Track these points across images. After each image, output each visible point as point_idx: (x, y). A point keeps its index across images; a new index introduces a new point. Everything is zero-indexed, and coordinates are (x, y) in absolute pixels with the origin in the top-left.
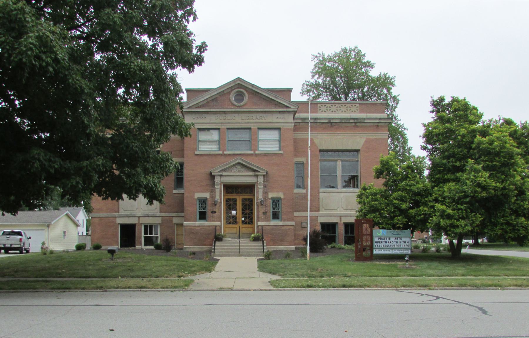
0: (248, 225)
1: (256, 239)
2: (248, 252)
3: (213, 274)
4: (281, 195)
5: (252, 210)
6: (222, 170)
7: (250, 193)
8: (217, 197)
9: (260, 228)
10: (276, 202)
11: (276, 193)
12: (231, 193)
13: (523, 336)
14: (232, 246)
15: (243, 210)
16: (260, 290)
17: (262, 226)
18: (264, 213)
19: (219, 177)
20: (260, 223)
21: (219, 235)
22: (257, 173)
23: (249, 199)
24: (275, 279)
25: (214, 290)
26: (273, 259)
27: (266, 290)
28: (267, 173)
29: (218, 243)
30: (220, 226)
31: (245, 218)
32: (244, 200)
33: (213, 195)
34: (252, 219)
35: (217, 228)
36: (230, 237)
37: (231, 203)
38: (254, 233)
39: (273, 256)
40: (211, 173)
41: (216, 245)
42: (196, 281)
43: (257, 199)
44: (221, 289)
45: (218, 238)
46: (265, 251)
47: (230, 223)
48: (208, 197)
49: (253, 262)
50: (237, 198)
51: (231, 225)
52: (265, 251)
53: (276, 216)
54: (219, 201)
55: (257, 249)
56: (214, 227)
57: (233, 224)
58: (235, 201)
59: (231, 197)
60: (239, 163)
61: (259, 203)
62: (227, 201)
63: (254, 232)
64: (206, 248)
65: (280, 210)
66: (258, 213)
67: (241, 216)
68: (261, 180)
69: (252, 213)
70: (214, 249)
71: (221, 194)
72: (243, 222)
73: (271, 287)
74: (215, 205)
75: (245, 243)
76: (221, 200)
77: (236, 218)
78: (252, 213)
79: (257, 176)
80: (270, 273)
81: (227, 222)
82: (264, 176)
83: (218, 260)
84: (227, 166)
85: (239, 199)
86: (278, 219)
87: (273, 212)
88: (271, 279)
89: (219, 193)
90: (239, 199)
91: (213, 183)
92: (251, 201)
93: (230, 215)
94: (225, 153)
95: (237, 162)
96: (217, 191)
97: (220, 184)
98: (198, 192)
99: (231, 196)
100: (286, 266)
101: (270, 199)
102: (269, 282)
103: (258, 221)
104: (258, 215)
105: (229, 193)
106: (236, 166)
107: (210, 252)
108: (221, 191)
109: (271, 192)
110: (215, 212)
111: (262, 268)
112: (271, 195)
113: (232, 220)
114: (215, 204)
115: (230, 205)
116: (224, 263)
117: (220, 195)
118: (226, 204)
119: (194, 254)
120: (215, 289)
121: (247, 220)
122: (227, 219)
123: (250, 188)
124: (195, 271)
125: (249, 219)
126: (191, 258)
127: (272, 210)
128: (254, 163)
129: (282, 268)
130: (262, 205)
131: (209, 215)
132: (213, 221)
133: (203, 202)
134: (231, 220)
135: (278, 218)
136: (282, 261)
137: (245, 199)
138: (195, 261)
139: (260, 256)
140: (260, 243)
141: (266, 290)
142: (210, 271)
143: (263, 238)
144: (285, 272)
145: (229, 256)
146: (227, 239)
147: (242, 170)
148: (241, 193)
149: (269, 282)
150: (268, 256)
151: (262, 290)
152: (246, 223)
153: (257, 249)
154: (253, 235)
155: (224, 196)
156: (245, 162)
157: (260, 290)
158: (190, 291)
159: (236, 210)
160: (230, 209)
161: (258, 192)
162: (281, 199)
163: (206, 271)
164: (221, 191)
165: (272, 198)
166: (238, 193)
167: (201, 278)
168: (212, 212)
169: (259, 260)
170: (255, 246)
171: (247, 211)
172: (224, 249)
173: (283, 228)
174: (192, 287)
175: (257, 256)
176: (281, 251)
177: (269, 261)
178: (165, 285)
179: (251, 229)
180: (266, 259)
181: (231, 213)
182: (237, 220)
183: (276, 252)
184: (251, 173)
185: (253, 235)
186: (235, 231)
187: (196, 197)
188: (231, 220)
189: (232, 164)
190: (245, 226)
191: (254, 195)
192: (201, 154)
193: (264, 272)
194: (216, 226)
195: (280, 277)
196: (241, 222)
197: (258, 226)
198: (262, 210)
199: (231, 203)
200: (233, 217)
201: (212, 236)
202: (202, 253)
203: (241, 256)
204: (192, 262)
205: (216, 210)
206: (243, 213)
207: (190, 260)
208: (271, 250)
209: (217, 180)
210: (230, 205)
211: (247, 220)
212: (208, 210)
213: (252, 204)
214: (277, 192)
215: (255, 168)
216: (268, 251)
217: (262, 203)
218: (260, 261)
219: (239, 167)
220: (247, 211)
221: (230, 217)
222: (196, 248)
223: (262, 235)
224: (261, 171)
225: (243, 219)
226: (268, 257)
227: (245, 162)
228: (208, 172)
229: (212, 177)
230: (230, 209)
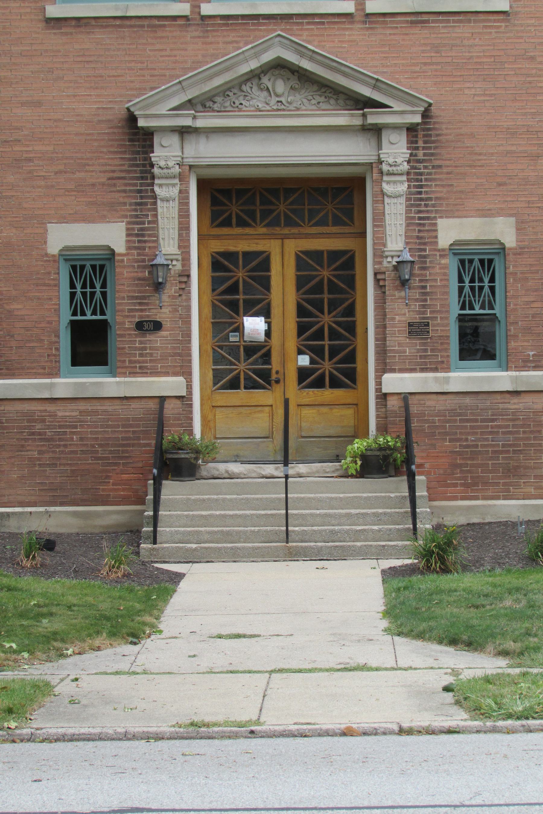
0: (328, 394)
1: (374, 465)
2: (332, 536)
3: (151, 652)
4: (503, 231)
5: (350, 311)
6: (190, 103)
7: (337, 222)
8: (168, 246)
9: (393, 403)
10: (479, 267)
11: (477, 221)
12: (242, 223)
13: (190, 810)
14: (247, 504)
15: (301, 311)
16: (402, 731)
17: (405, 397)
18: (418, 329)
19: (175, 139)
20: (396, 382)
21: (178, 447)
22: (375, 118)
23: (334, 255)
24: (479, 673)
25: (159, 737)
26: (465, 568)
27: (430, 731)
28: (426, 114)
29: (172, 490)
30: (185, 400)
31: (317, 353)
32: (306, 261)
33: (142, 234)
34: (351, 357)
35: (170, 408)
36: (237, 459)
37: (241, 274)
38: (366, 434)
39: (464, 554)
40: (132, 119)
41: (164, 496)
42: (65, 689)
43: (379, 255)
44: (196, 731)
45: (176, 463)
46: (425, 526)
47: (234, 385)
48: (120, 247)
49: (356, 589)
50: (272, 247)
51: (241, 395)
52: (425, 526)
53: (477, 342)
54: (178, 266)
55: (378, 519)
56: (153, 405)
57: (252, 385)
58: (260, 264)
59: (242, 246)
60: (279, 66)
61: (390, 275)
62: (219, 265)
63: (361, 431)
64: (111, 515)
65: (498, 311)
66: (381, 327)
67: (292, 343)
68: (396, 151)
69: (350, 312)
70: (155, 518)
71: (184, 228)
72: (303, 374)
73: (459, 718)
74: (158, 287)
75: (318, 487)
76: (186, 260)
77: (267, 357)
78: (351, 328)
79: (376, 131)
80: (453, 642)
81: (217, 376)
82: (411, 129)
83: (178, 577)
84: (217, 82)
85: (283, 256)
86: (492, 357)
87: (461, 318)
88: (455, 672)
89: (175, 234)
90: (283, 256)
91: (146, 172)
92: (347, 265)
93: (234, 338)
94: (207, 9)
95: (267, 57)
96: (167, 215)
97: (182, 177)
98: (63, 219)
99: (242, 242)
100: (531, 606)
101: (443, 253)
102: (447, 689)
103: (384, 367)
104: (382, 339)
105: (227, 223)
106: (266, 81)
107: (132, 534)
108: (184, 215)
109: (449, 214)
110: (157, 326)
111: (407, 617)
112: (450, 231)
113: (243, 369)
114: (154, 280)
115: (233, 289)
116: (208, 595)
117: (179, 231)
118: (216, 283)
119: (49, 545)
120: (165, 729)
121: (327, 366)
122: (217, 359)
123: (339, 196)
124: (55, 636)
125: (336, 362)
126: (35, 570)
127: (455, 310)
128: (357, 60)
129: (514, 615)
130: (404, 283)
131: (122, 338)
132: (144, 372)
133: (90, 272)
134: (242, 367)
135: (489, 355)
136: (512, 580)
137: (316, 255)
138: (57, 586)
139: (397, 553)
140: (394, 488)
141: (430, 731)
142: (135, 637)
143: (409, 460)
144: (528, 633)
145: (235, 556)
146: (222, 467)
147: (297, 99)
148: (290, 223)
149: (447, 689)
150: (438, 555)
151: (409, 732)
152: (319, 384)
153: (378, 519)
154: (359, 445)
155: (201, 237)
156: (313, 56)
157: (402, 731)
158: (31, 739)
159: (266, 313)
160: (233, 306)
161: (380, 218)
162: (502, 249)
163: (113, 634)
164: (184, 215)
165: (456, 248)
166: (275, 223)
167: (90, 676)
168: (140, 326)
169: (389, 574)
170: (368, 503)
171: (326, 320)
172: (206, 520)
173: (515, 404)
174: (42, 722)
175: (381, 553)
176: (506, 528)
177: (445, 581)
178: (110, 764)
179: (349, 412)
180: (428, 569)
181: (239, 329)
182: (275, 364)
183: (480, 531)
184: (343, 118)
185: (359, 445)
186: (260, 423)
187: (54, 247)
188: (242, 367)
189: (244, 69)
190: (313, 395)
191: (363, 234)
192: (79, 22)
193: (420, 636)
194: (162, 399)
195: (502, 662)
196: (292, 377)
197: (383, 397)
198: (402, 312)
199: (241, 274)
200: (252, 349)
201: (144, 451)
202: (88, 541)
203: (293, 555)
204: (38, 588)
205: (163, 315)
206: (301, 329)
207: (27, 581)
208: (452, 520)
209: (166, 153)
210: (236, 286)
211: (327, 366)
212: (121, 315)
213: (351, 282)
214: (485, 213)
215: (366, 92)
216: (438, 528)
217: (402, 276)
218: (396, 583)
219: (280, 86)
220: (326, 320)
221: (233, 350)
222: (60, 519)
223: (408, 446)
224: (397, 106)
225: (304, 361)
226: (442, 559)
227: (313, 56)
228: (118, 112)
229: (138, 138)
230: (233, 306)
